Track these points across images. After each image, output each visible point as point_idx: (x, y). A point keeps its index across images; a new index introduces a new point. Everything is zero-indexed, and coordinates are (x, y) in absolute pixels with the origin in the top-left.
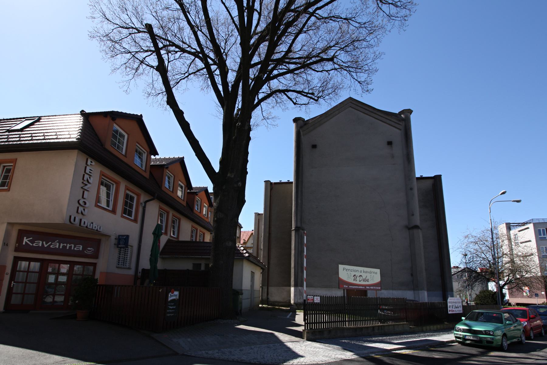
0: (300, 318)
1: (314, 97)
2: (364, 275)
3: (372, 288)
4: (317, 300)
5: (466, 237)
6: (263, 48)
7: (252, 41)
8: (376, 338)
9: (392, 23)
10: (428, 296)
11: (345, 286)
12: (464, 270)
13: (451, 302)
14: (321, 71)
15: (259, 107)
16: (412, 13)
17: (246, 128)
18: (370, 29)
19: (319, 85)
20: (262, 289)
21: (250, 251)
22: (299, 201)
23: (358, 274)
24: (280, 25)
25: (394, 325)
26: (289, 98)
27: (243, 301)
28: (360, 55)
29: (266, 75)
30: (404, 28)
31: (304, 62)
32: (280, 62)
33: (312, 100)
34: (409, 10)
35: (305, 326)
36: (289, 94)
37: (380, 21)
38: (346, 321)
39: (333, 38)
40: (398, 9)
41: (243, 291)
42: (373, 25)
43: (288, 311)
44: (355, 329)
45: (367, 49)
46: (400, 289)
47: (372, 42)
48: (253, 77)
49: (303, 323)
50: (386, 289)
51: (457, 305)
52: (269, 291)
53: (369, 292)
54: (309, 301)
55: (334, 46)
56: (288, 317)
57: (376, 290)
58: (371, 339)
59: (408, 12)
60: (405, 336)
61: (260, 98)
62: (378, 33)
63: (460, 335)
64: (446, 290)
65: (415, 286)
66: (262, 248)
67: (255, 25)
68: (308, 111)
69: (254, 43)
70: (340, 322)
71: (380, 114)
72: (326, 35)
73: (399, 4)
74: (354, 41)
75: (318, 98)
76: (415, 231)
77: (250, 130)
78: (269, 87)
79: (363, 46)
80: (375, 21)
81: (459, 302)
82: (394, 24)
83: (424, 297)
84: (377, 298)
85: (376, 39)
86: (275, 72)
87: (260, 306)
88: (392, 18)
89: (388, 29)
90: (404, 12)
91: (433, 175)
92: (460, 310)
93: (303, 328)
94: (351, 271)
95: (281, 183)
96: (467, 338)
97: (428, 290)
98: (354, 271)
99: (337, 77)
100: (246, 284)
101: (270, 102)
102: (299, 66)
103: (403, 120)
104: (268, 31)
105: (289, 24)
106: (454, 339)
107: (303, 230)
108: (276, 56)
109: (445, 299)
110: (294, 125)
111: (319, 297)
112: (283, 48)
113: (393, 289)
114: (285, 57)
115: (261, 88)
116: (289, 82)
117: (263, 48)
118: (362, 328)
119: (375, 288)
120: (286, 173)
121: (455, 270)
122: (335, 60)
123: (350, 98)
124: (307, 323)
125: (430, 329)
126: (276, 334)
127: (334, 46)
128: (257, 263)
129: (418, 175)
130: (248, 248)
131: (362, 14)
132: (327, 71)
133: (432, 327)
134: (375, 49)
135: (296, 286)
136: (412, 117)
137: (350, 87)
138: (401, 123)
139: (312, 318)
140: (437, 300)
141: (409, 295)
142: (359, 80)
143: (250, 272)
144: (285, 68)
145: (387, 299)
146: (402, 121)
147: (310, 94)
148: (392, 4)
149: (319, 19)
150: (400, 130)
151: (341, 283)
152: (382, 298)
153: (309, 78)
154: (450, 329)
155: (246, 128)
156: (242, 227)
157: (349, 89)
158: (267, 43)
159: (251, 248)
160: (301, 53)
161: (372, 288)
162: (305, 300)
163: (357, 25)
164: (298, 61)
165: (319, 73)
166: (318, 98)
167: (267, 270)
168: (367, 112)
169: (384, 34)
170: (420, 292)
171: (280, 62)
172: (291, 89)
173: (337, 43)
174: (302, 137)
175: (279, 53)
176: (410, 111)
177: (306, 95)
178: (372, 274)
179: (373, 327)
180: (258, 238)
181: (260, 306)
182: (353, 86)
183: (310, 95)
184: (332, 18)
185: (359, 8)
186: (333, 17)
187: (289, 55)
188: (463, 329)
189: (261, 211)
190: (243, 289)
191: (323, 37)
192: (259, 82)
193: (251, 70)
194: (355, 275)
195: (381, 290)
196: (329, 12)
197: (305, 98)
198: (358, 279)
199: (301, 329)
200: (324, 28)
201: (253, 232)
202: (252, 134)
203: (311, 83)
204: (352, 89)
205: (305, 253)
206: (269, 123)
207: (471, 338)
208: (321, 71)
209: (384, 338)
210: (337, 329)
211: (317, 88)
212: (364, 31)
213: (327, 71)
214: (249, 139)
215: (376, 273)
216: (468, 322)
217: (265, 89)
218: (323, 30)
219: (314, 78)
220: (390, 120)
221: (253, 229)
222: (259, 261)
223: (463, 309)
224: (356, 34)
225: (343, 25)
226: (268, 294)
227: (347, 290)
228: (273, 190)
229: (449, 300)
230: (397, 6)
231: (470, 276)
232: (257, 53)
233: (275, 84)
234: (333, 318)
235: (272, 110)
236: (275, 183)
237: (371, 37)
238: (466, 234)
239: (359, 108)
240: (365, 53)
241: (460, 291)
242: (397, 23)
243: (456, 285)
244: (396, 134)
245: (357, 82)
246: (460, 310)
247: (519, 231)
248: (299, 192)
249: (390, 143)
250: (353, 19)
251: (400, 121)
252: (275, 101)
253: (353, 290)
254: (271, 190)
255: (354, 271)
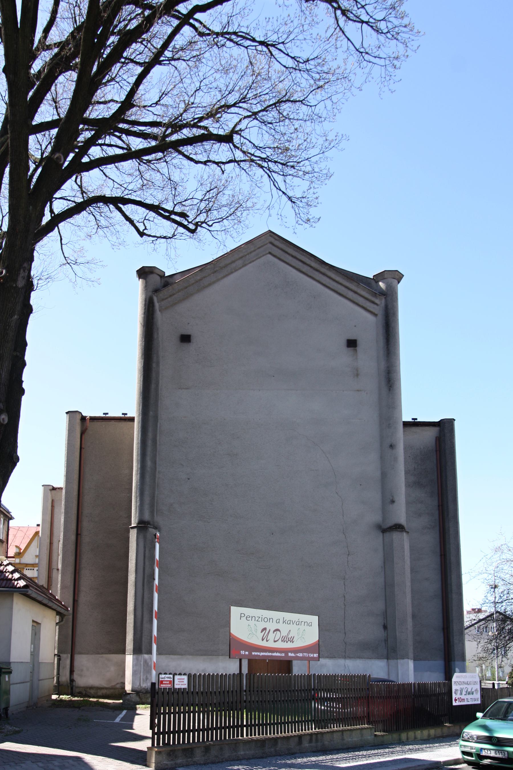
0: (142, 722)
1: (186, 223)
2: (285, 629)
3: (300, 655)
4: (181, 683)
5: (498, 549)
6: (66, 84)
7: (37, 66)
8: (305, 760)
9: (367, 70)
10: (416, 669)
11: (243, 652)
12: (489, 618)
13: (460, 683)
14: (205, 163)
15: (55, 233)
16: (409, 53)
17: (21, 283)
18: (317, 76)
19: (199, 195)
20: (59, 660)
21: (29, 573)
22: (149, 463)
23: (271, 626)
24: (105, 37)
25: (342, 731)
26: (127, 218)
27: (12, 688)
28: (294, 136)
29: (71, 156)
30: (392, 87)
31: (165, 136)
32: (104, 127)
33: (181, 230)
34: (405, 44)
35: (153, 738)
36: (128, 209)
37: (340, 62)
38: (242, 726)
39: (235, 85)
40: (382, 38)
41: (13, 667)
42: (325, 69)
43: (118, 708)
44: (262, 743)
45: (308, 123)
46: (360, 657)
47: (320, 109)
48: (38, 155)
49: (149, 733)
50: (331, 656)
51: (470, 688)
52: (76, 664)
53: (295, 663)
54: (163, 686)
55: (234, 105)
56: (118, 720)
57: (309, 659)
58: (293, 761)
59: (401, 46)
60: (365, 753)
61: (56, 211)
62: (334, 88)
63: (472, 748)
64: (450, 657)
65: (390, 650)
66: (60, 566)
67: (45, 23)
68: (172, 253)
69: (39, 72)
70: (259, 725)
71: (338, 279)
72: (218, 76)
73: (382, 26)
74: (280, 102)
75: (197, 225)
76: (396, 535)
77: (30, 287)
78: (80, 187)
79: (301, 116)
80: (329, 58)
81: (475, 683)
82: (369, 73)
83: (408, 672)
84: (309, 676)
85: (328, 103)
86: (95, 152)
87: (54, 697)
88: (367, 57)
89: (357, 84)
90: (391, 47)
91: (436, 419)
92: (476, 699)
93: (148, 743)
94: (258, 619)
95: (105, 419)
96: (484, 753)
97: (415, 659)
98: (263, 620)
99: (243, 182)
100: (20, 651)
101: (83, 224)
102: (153, 143)
103: (383, 294)
104: (76, 46)
105: (129, 37)
106: (460, 756)
107: (156, 528)
108: (97, 112)
109: (449, 676)
110: (139, 284)
111: (185, 678)
112: (110, 95)
113: (345, 657)
114: (119, 115)
115: (59, 188)
116: (129, 179)
117: (66, 84)
118: (276, 740)
119: (306, 654)
120: (119, 396)
121: (473, 616)
122: (236, 138)
123: (270, 233)
124: (159, 733)
125: (415, 738)
126: (88, 758)
127: (234, 105)
128: (45, 601)
129: (407, 417)
130: (27, 565)
131: (301, 37)
132: (217, 163)
133: (418, 733)
134: (326, 125)
135: (137, 650)
136: (402, 288)
137: (268, 208)
138: (377, 301)
139: (169, 721)
140: (432, 677)
141: (376, 669)
142: (290, 194)
143: (31, 623)
144: (120, 143)
145: (333, 678)
146: (378, 294)
147: (176, 214)
148: (367, 23)
149: (201, 34)
150: (375, 315)
151: (233, 647)
152: (319, 677)
153: (176, 177)
154: (454, 736)
155: (21, 283)
156: (11, 518)
157: (262, 210)
158: (74, 75)
159: (33, 565)
160: (158, 110)
161: (300, 655)
162: (153, 684)
163: (290, 63)
164: (148, 130)
165: (200, 165)
166: (197, 225)
167: (71, 617)
168: (305, 269)
169: (348, 94)
170: (400, 661)
171: (104, 127)
172: (133, 198)
173: (244, 99)
174: (158, 315)
175: (105, 103)
176: (397, 276)
177: (168, 215)
178: (302, 627)
179: (300, 737)
180: (51, 543)
181: (54, 697)
182: (276, 206)
183: (178, 218)
184: (233, 37)
185: (296, 22)
186: (235, 33)
187: (129, 113)
188: (478, 737)
189: (60, 482)
190: (12, 660)
191: (211, 79)
192: (55, 174)
193: (32, 139)
194: (265, 629)
195: (318, 659)
196: (225, 21)
197: (167, 223)
198: (271, 636)
199: (143, 746)
200: (212, 57)
201: (40, 529)
202: (35, 299)
203: (179, 189)
204: (273, 212)
205: (156, 582)
206: (79, 274)
207: (493, 754)
208: (205, 163)
209: (321, 758)
210: (222, 744)
211: (196, 201)
212: (304, 81)
213: (217, 163)
214: (28, 310)
215: (310, 625)
216: (489, 722)
217: (69, 192)
218: (210, 64)
219: (186, 177)
220: (356, 293)
221: (40, 522)
222: (52, 598)
223: (482, 696)
224: (287, 83)
225: (259, 56)
226: (72, 671)
227: (250, 662)
228: (87, 432)
229: (454, 679)
230: (378, 31)
231: (500, 630)
232: (48, 96)
233: (94, 181)
234: (215, 720)
235: (86, 244)
236: (93, 419)
237: (319, 97)
238: (497, 544)
239: (289, 259)
240: (303, 131)
241: (480, 659)
242: (377, 71)
243: (472, 648)
244: (364, 323)
245: (284, 198)
246: (476, 699)
247: (271, 243)
248: (149, 443)
249: (352, 344)
250: (281, 46)
251: (375, 295)
252: (93, 222)
253: (262, 661)
254: (82, 433)
255: (263, 620)
